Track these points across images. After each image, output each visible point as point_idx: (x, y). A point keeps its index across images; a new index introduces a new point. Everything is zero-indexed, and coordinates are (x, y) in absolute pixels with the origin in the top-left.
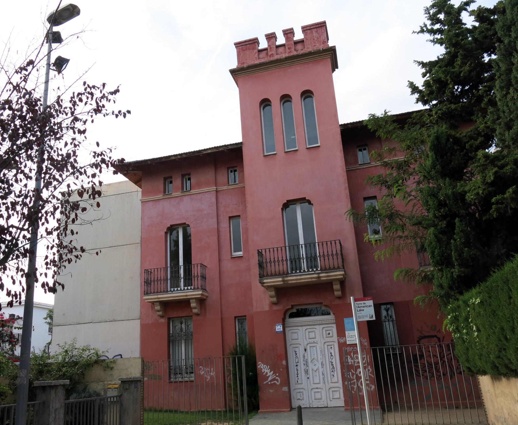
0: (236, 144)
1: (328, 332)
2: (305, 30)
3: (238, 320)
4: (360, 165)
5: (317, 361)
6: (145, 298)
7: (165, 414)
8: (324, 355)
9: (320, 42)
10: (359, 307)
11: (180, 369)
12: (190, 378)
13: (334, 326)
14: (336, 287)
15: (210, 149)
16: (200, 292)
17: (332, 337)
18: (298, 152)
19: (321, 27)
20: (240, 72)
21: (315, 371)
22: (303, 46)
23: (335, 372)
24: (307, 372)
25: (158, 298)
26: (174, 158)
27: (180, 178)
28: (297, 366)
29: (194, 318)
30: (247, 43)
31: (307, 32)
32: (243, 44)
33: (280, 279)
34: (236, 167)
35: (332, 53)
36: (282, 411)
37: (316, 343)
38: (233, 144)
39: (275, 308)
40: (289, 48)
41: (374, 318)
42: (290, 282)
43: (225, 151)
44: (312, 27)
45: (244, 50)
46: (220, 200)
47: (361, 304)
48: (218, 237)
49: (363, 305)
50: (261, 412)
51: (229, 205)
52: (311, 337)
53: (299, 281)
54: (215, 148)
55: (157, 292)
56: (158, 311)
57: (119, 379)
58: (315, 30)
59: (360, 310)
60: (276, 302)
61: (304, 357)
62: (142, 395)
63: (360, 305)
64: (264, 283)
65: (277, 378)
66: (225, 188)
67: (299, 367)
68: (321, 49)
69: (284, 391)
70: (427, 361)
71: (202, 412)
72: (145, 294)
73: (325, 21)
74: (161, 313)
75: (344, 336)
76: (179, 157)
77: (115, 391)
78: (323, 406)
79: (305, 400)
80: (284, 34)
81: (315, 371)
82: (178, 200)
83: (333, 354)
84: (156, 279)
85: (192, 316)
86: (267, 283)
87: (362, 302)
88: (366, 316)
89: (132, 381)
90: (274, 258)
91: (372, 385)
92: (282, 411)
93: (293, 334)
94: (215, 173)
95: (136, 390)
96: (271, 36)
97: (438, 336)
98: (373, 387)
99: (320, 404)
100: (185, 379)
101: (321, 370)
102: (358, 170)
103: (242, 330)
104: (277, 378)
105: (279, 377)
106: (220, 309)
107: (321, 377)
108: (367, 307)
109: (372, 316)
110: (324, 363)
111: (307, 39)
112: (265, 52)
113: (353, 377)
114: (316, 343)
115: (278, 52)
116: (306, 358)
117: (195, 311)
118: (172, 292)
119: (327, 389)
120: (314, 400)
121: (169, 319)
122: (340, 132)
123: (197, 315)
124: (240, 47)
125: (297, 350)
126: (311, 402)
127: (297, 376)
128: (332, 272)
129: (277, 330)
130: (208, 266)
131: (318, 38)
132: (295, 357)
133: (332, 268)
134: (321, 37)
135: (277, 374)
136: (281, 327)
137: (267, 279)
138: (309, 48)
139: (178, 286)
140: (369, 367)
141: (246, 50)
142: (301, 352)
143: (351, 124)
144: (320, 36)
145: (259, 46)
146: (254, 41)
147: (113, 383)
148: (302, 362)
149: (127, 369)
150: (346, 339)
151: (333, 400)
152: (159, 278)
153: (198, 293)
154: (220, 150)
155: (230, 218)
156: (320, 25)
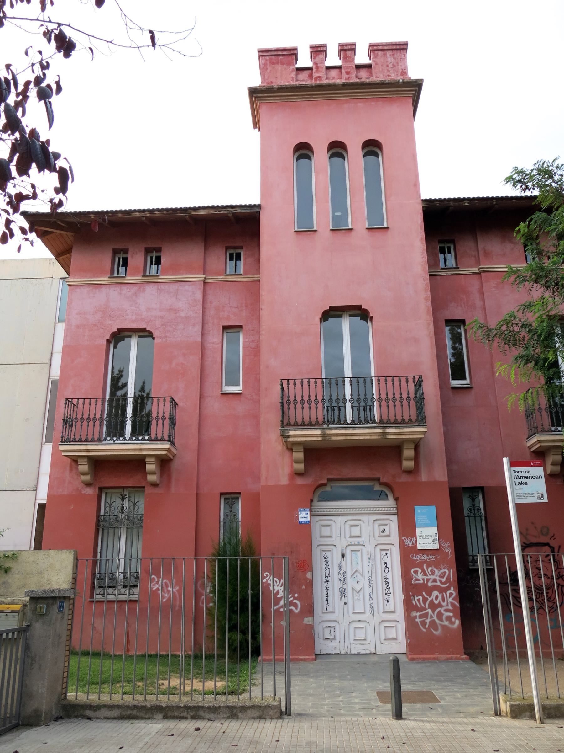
0: (250, 206)
1: (382, 528)
2: (375, 50)
3: (225, 499)
4: (442, 269)
5: (362, 575)
6: (62, 448)
7: (84, 659)
8: (373, 566)
9: (397, 72)
10: (518, 477)
11: (113, 578)
12: (119, 596)
13: (395, 518)
14: (408, 452)
15: (204, 208)
16: (167, 446)
17: (389, 536)
18: (353, 233)
19: (400, 49)
20: (266, 95)
21: (358, 592)
22: (368, 74)
23: (391, 595)
24: (343, 593)
25: (88, 451)
26: (138, 215)
27: (143, 253)
28: (327, 582)
29: (148, 490)
30: (280, 53)
31: (378, 54)
32: (273, 53)
33: (318, 432)
34: (241, 248)
35: (415, 91)
36: (301, 660)
37: (361, 545)
38: (245, 206)
39: (300, 481)
40: (348, 73)
41: (545, 500)
42: (333, 438)
43: (230, 215)
44: (386, 48)
45: (273, 64)
46: (210, 298)
47: (522, 472)
48: (202, 357)
49: (525, 474)
50: (264, 660)
51: (224, 306)
52: (353, 534)
53: (349, 438)
54: (213, 207)
55: (87, 440)
56: (84, 474)
57: (27, 593)
58: (391, 52)
59: (521, 484)
60: (303, 472)
61: (340, 567)
62: (69, 627)
63: (520, 475)
64: (289, 436)
65: (295, 601)
66: (220, 278)
67: (330, 585)
68: (401, 81)
69: (306, 625)
70: (534, 583)
71: (150, 656)
72: (62, 442)
73: (407, 42)
74: (87, 478)
75: (414, 535)
76: (148, 214)
77: (14, 617)
78: (368, 652)
79: (338, 640)
80: (341, 50)
81: (358, 592)
82: (135, 288)
83: (389, 565)
84: (86, 416)
85: (144, 487)
86: (295, 436)
87: (524, 469)
88: (532, 495)
89: (55, 598)
90: (309, 396)
91: (456, 619)
92: (301, 660)
93: (323, 528)
94: (205, 253)
95: (60, 616)
96: (319, 49)
97: (551, 545)
98: (457, 622)
99: (363, 647)
100: (108, 596)
101: (367, 590)
102: (438, 277)
103: (231, 518)
104: (295, 601)
105: (300, 601)
106: (196, 478)
107: (368, 602)
108: (532, 477)
109: (542, 495)
110: (374, 579)
111: (376, 64)
112: (307, 73)
113: (425, 605)
114: (361, 545)
115: (329, 76)
116: (344, 569)
117: (152, 478)
118: (114, 441)
119: (377, 623)
120: (352, 642)
121: (101, 489)
122: (421, 211)
123: (155, 485)
124: (267, 58)
125: (328, 554)
126: (347, 644)
127: (327, 600)
128: (406, 427)
129: (300, 519)
130: (180, 404)
131: (394, 65)
132: (324, 567)
133: (407, 420)
134: (400, 64)
135: (296, 595)
136: (307, 514)
137: (295, 430)
138: (378, 76)
139: (122, 433)
140: (452, 588)
141: (277, 63)
142: (335, 558)
143: (440, 200)
144: (398, 63)
145: (296, 63)
146: (292, 52)
147: (9, 599)
148: (336, 576)
149: (40, 573)
150: (416, 541)
151: (386, 642)
152: (92, 416)
153: (162, 447)
154: (222, 212)
155: (225, 328)
156: (398, 47)
